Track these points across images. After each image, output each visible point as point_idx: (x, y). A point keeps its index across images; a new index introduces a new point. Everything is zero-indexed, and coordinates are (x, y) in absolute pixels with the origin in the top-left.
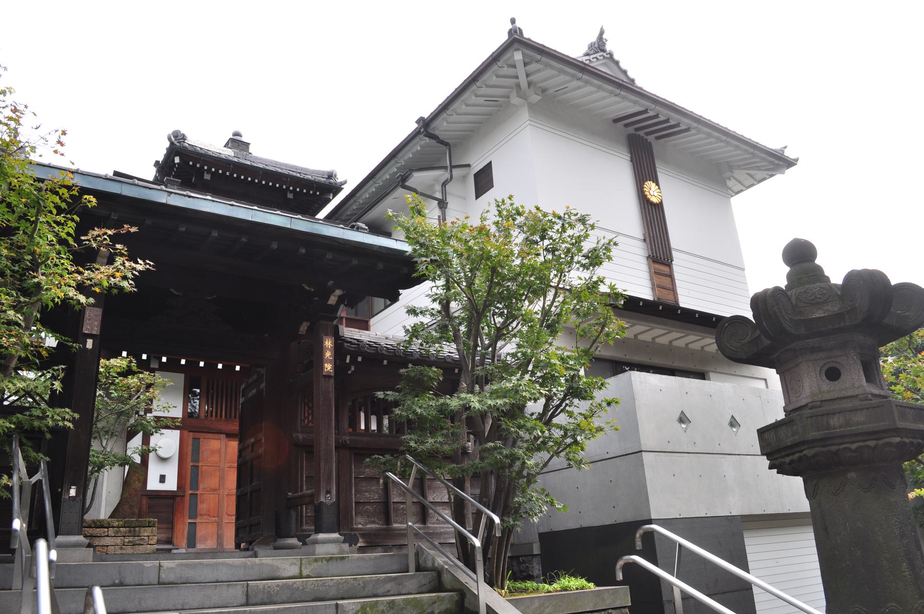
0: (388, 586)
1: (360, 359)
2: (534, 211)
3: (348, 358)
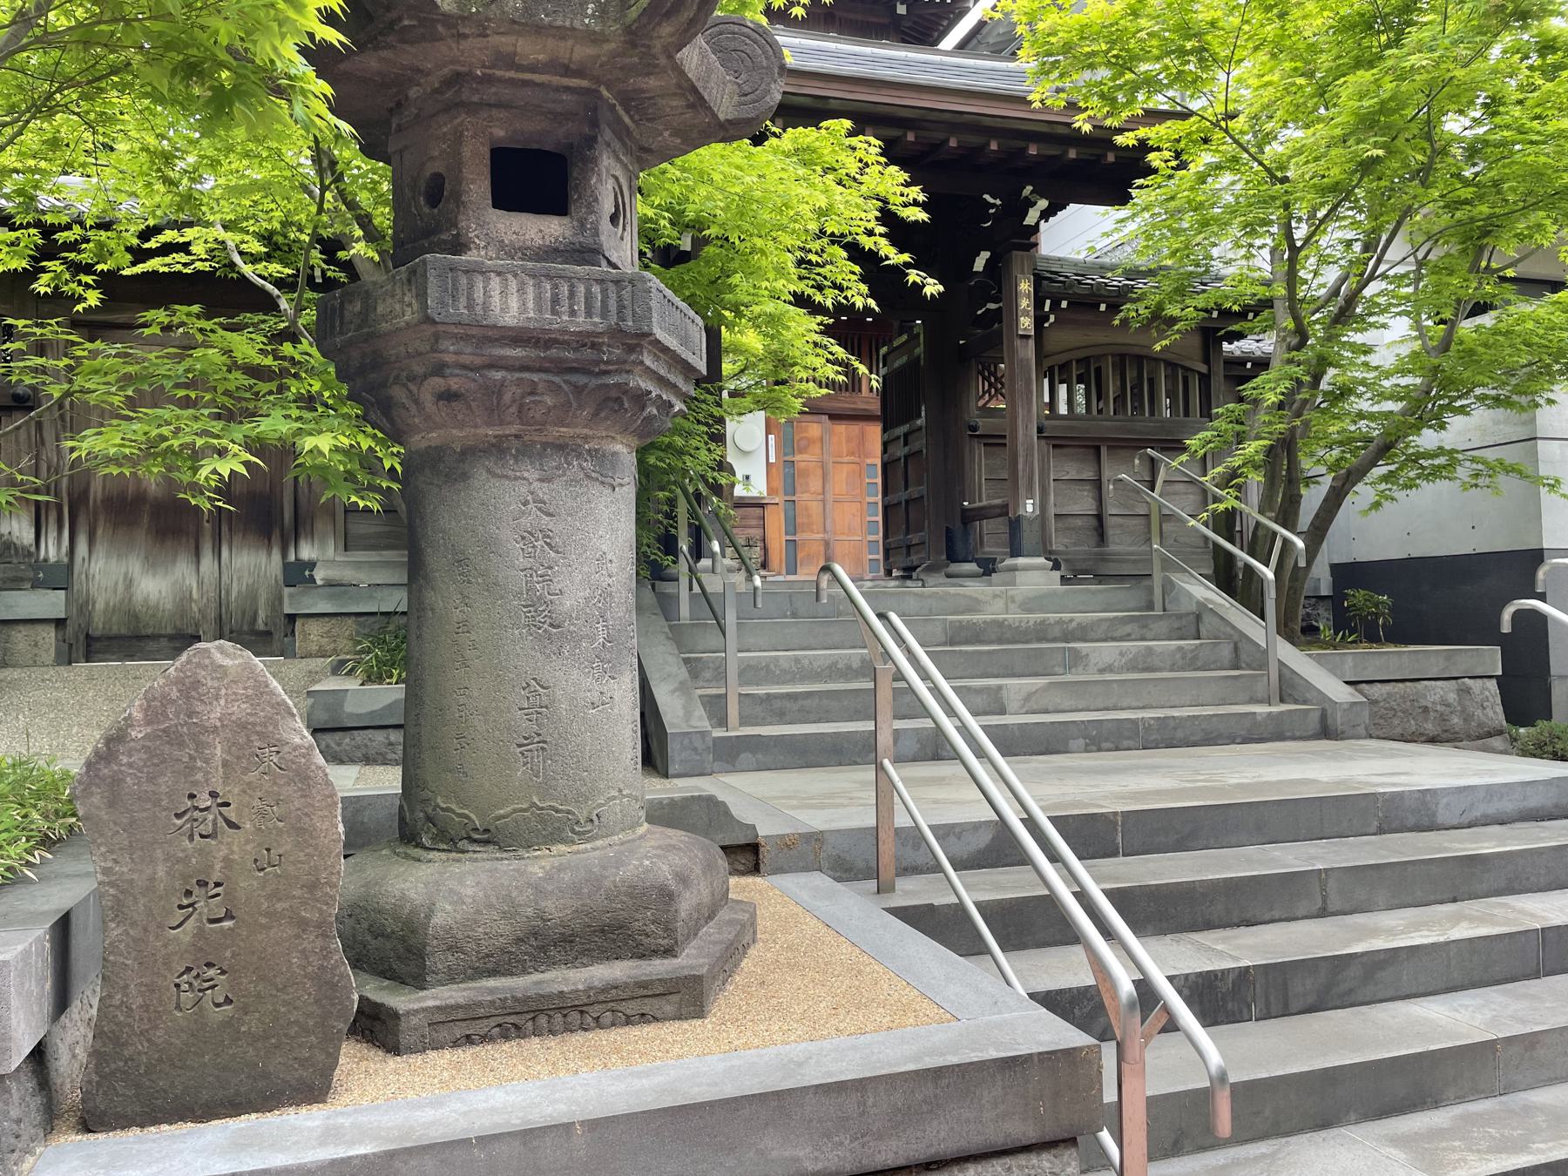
0: (1128, 629)
1: (1064, 304)
2: (1551, 396)
3: (1048, 302)
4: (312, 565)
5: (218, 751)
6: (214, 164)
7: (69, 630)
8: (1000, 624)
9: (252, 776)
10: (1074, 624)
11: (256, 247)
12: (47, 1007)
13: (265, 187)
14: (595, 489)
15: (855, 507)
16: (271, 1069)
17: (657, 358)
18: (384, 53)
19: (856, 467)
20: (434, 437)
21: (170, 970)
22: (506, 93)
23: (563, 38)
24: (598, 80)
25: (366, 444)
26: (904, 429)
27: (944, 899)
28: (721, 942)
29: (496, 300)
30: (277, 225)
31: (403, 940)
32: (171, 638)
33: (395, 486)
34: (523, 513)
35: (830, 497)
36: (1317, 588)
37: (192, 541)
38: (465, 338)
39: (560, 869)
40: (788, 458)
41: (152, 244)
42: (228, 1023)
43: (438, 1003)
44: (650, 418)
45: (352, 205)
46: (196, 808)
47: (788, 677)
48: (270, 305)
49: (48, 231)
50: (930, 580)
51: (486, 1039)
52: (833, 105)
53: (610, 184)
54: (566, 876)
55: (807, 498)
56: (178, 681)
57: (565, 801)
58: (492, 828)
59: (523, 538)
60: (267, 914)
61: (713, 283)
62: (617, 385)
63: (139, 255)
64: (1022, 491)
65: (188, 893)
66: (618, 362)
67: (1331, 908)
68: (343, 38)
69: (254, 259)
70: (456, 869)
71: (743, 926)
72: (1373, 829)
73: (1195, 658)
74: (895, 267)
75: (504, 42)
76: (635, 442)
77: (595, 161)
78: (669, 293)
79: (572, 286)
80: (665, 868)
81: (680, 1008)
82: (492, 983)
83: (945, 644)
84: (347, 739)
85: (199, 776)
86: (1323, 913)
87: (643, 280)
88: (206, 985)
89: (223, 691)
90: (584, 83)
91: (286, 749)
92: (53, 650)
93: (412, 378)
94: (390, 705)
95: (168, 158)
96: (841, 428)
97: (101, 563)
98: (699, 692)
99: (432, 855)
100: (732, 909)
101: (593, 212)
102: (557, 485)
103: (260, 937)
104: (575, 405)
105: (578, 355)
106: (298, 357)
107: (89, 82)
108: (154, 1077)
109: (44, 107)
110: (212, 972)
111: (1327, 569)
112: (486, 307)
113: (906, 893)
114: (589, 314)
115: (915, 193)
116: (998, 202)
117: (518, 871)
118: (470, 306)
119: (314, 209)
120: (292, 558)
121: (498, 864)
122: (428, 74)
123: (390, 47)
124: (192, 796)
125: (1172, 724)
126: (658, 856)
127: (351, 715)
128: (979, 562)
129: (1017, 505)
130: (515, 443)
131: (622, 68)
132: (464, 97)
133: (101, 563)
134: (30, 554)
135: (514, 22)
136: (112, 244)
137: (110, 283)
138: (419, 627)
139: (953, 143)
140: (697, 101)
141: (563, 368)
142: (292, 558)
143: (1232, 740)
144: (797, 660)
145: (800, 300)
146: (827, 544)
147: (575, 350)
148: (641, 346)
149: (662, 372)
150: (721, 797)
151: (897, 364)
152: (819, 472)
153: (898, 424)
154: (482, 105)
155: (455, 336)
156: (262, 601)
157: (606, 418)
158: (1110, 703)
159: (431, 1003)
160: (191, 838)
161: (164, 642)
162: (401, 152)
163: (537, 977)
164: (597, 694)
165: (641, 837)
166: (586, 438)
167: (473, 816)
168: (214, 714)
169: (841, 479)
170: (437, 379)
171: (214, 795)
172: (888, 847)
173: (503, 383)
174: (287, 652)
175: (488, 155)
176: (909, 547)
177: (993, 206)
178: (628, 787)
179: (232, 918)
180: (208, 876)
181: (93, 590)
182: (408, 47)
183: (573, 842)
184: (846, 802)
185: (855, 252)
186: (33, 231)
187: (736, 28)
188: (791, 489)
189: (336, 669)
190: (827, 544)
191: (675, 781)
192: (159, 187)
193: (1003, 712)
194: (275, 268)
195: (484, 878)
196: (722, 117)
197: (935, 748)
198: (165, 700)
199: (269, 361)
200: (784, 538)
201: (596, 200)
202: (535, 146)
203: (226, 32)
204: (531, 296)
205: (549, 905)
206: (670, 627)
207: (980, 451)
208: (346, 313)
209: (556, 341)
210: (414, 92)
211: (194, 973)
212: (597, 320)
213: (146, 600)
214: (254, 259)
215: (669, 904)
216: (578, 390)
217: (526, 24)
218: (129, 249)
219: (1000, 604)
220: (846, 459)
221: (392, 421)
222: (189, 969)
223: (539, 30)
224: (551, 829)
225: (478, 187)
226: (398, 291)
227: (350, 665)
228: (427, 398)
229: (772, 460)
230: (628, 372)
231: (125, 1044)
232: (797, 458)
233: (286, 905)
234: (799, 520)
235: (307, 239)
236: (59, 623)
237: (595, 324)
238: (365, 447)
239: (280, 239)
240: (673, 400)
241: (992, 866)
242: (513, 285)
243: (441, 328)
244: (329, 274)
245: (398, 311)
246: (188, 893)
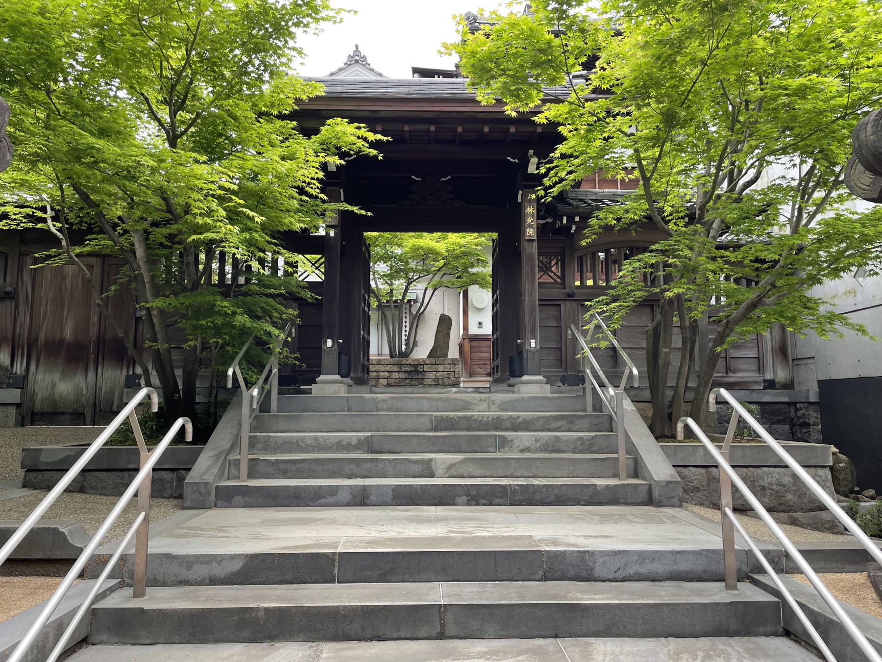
0: (559, 423)
3: (565, 218)
10: (520, 420)
32: (71, 414)
36: (808, 397)
47: (310, 449)
64: (528, 334)
67: (448, 633)
72: (539, 576)
73: (592, 445)
83: (431, 430)
86: (441, 636)
97: (41, 375)
111: (816, 383)
125: (532, 490)
133: (41, 375)
134: (8, 370)
143: (577, 502)
144: (316, 438)
156: (116, 395)
158: (508, 473)
161: (68, 416)
181: (37, 389)
193: (432, 476)
219: (484, 405)
236: (18, 406)
241: (241, 584)
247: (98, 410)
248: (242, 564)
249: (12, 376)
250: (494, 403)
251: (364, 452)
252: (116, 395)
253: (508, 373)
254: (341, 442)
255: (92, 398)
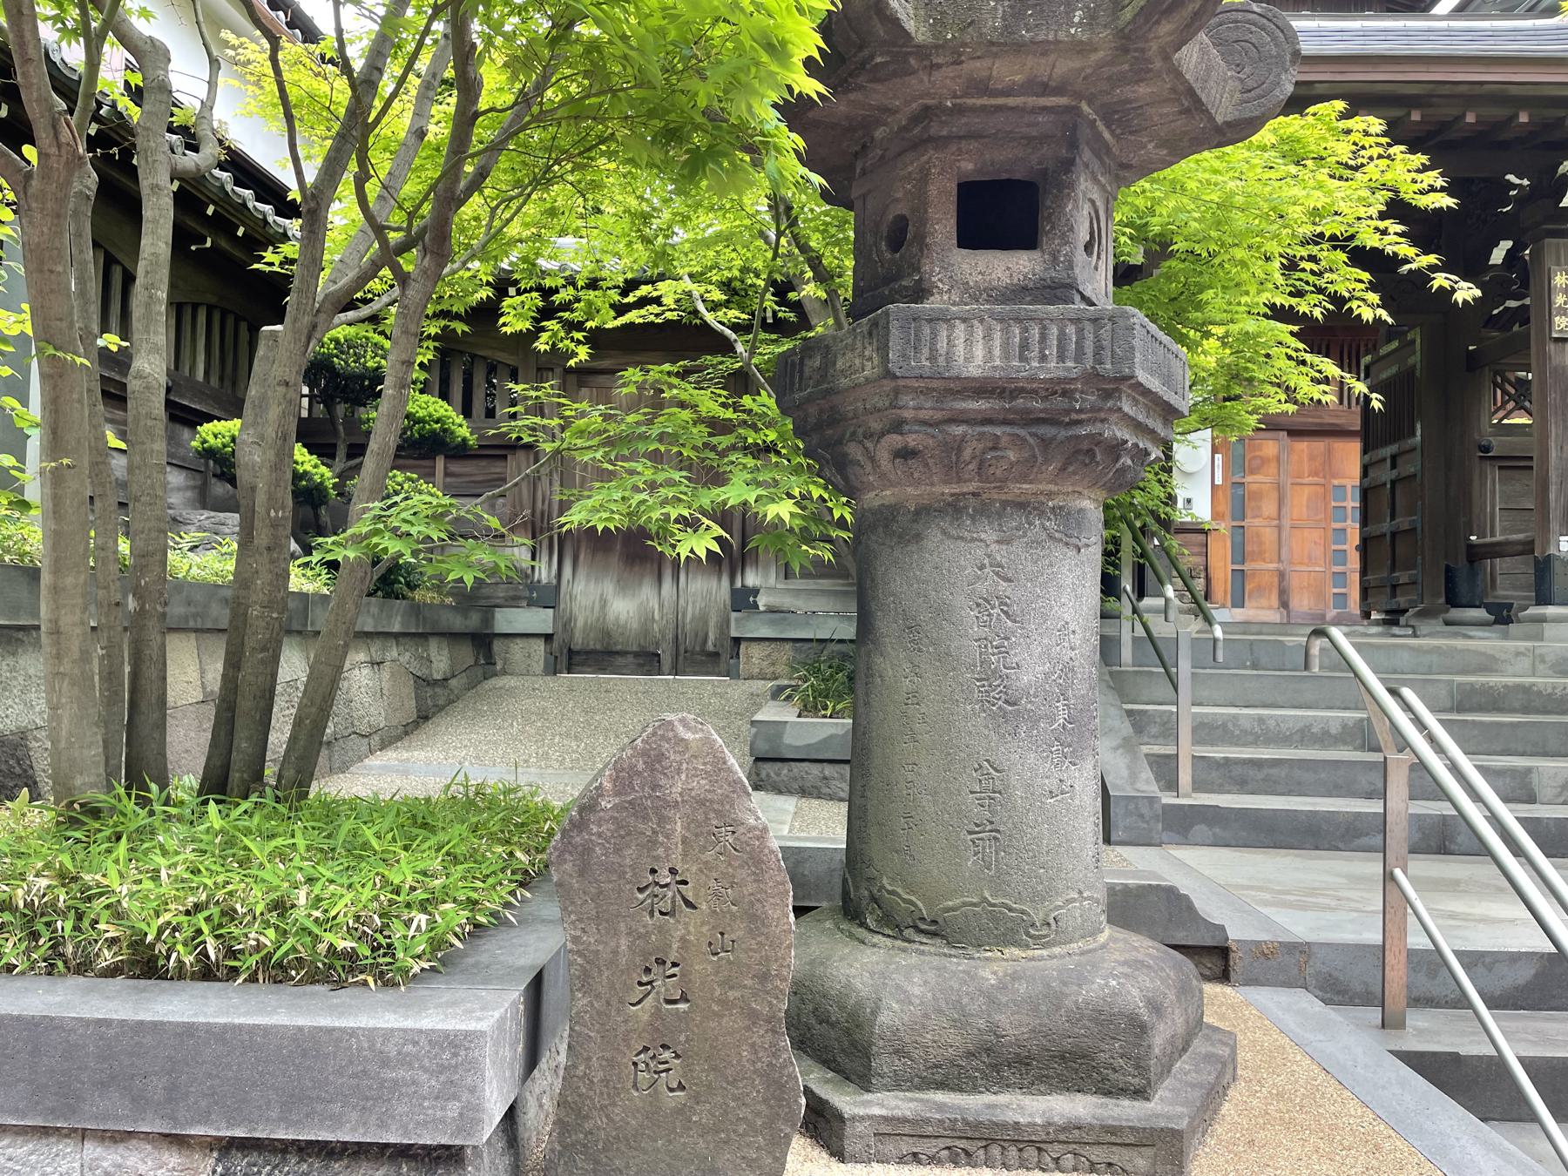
4: (755, 592)
5: (679, 827)
6: (685, 220)
7: (555, 644)
8: (1526, 690)
9: (709, 855)
11: (717, 295)
12: (518, 1069)
13: (726, 238)
14: (1058, 551)
15: (1316, 535)
16: (720, 1165)
17: (1136, 402)
18: (852, 96)
19: (1320, 490)
20: (888, 495)
21: (628, 1046)
22: (976, 122)
23: (1044, 54)
24: (1078, 96)
25: (816, 492)
26: (1387, 451)
27: (1472, 1047)
28: (1200, 1085)
29: (960, 350)
30: (736, 273)
31: (847, 1032)
32: (637, 655)
33: (844, 535)
34: (979, 578)
35: (1286, 523)
37: (656, 566)
38: (926, 392)
39: (1015, 977)
40: (1237, 479)
41: (631, 299)
42: (680, 1111)
43: (884, 1112)
44: (1123, 471)
45: (804, 249)
46: (657, 884)
48: (726, 348)
49: (547, 293)
50: (1424, 627)
51: (934, 1160)
52: (1320, 89)
53: (1086, 209)
54: (1022, 988)
55: (1259, 524)
56: (644, 753)
57: (1020, 900)
58: (940, 920)
59: (978, 605)
60: (720, 1002)
61: (1172, 300)
62: (1089, 436)
63: (621, 310)
65: (648, 970)
66: (1092, 410)
68: (822, 89)
69: (714, 307)
70: (903, 960)
71: (1224, 1064)
74: (1418, 272)
75: (976, 68)
76: (1101, 495)
77: (1072, 186)
78: (1153, 327)
79: (1044, 328)
80: (1135, 992)
81: (1154, 1164)
82: (940, 1097)
84: (784, 769)
85: (661, 851)
87: (1127, 316)
88: (662, 1067)
89: (684, 766)
90: (1063, 101)
91: (741, 830)
92: (542, 663)
93: (869, 435)
94: (825, 740)
95: (645, 218)
96: (1303, 446)
98: (1145, 749)
99: (877, 939)
100: (1207, 1038)
101: (1067, 243)
102: (1017, 547)
103: (712, 1024)
104: (1040, 459)
105: (1047, 405)
106: (755, 408)
107: (580, 154)
108: (610, 1154)
109: (543, 180)
110: (667, 1055)
112: (949, 357)
113: (1420, 1032)
114: (1061, 357)
115: (1434, 178)
116: (1526, 182)
117: (967, 973)
118: (933, 358)
119: (770, 255)
120: (738, 584)
121: (945, 961)
122: (896, 112)
123: (860, 88)
124: (653, 871)
126: (1126, 976)
127: (790, 746)
128: (1490, 608)
129: (1546, 543)
130: (972, 500)
131: (1109, 78)
132: (932, 132)
134: (527, 576)
135: (992, 43)
136: (599, 303)
137: (597, 339)
138: (867, 694)
139: (1470, 118)
140: (1192, 103)
141: (1029, 420)
142: (738, 584)
144: (1261, 720)
145: (1280, 314)
146: (1282, 575)
147: (1044, 399)
148: (1117, 390)
149: (1141, 418)
150: (1184, 885)
151: (1384, 376)
152: (1275, 495)
153: (1385, 443)
154: (949, 139)
155: (915, 390)
156: (712, 624)
157: (1075, 473)
159: (877, 1111)
160: (652, 914)
161: (630, 659)
162: (864, 197)
163: (988, 1098)
164: (1056, 781)
165: (1103, 946)
166: (1050, 495)
167: (920, 905)
168: (676, 788)
169: (1300, 502)
170: (895, 436)
171: (673, 871)
172: (1397, 974)
173: (963, 439)
174: (733, 673)
175: (955, 192)
176: (1394, 587)
177: (1514, 186)
178: (1089, 888)
179: (687, 1001)
180: (667, 954)
181: (576, 610)
182: (878, 87)
183: (1027, 947)
184: (1333, 903)
185: (1361, 257)
186: (535, 294)
187: (1240, 16)
188: (1240, 512)
189: (776, 693)
190: (1282, 575)
191: (1119, 849)
192: (639, 246)
194: (733, 314)
195: (931, 975)
196: (1219, 119)
197: (1445, 839)
198: (633, 772)
199: (729, 414)
200: (1230, 567)
201: (1071, 229)
202: (1005, 176)
203: (705, 94)
204: (997, 342)
205: (1002, 1019)
206: (1111, 673)
207: (1493, 475)
208: (806, 370)
209: (1022, 390)
210: (879, 133)
211: (651, 1053)
212: (1070, 364)
213: (617, 619)
214: (714, 307)
215: (1141, 1038)
216: (1045, 443)
217: (1005, 44)
218: (612, 306)
219: (1525, 663)
220: (1306, 480)
221: (846, 479)
222: (646, 1049)
223: (1019, 48)
224: (1005, 930)
225: (943, 226)
226: (859, 344)
227: (788, 691)
228: (884, 456)
229: (1219, 481)
230: (1102, 421)
231: (587, 1117)
232: (1249, 479)
233: (737, 994)
234: (1248, 548)
235: (762, 284)
236: (548, 638)
237: (1068, 369)
238: (815, 495)
239: (737, 284)
240: (1150, 446)
242: (979, 332)
243: (901, 383)
244: (780, 315)
245: (859, 365)
246: (648, 970)
247: (682, 649)
248: (1533, 972)
249: (533, 586)
250: (1543, 661)
251: (1356, 749)
252: (712, 624)
253: (1442, 600)
254: (1309, 727)
255: (671, 626)
